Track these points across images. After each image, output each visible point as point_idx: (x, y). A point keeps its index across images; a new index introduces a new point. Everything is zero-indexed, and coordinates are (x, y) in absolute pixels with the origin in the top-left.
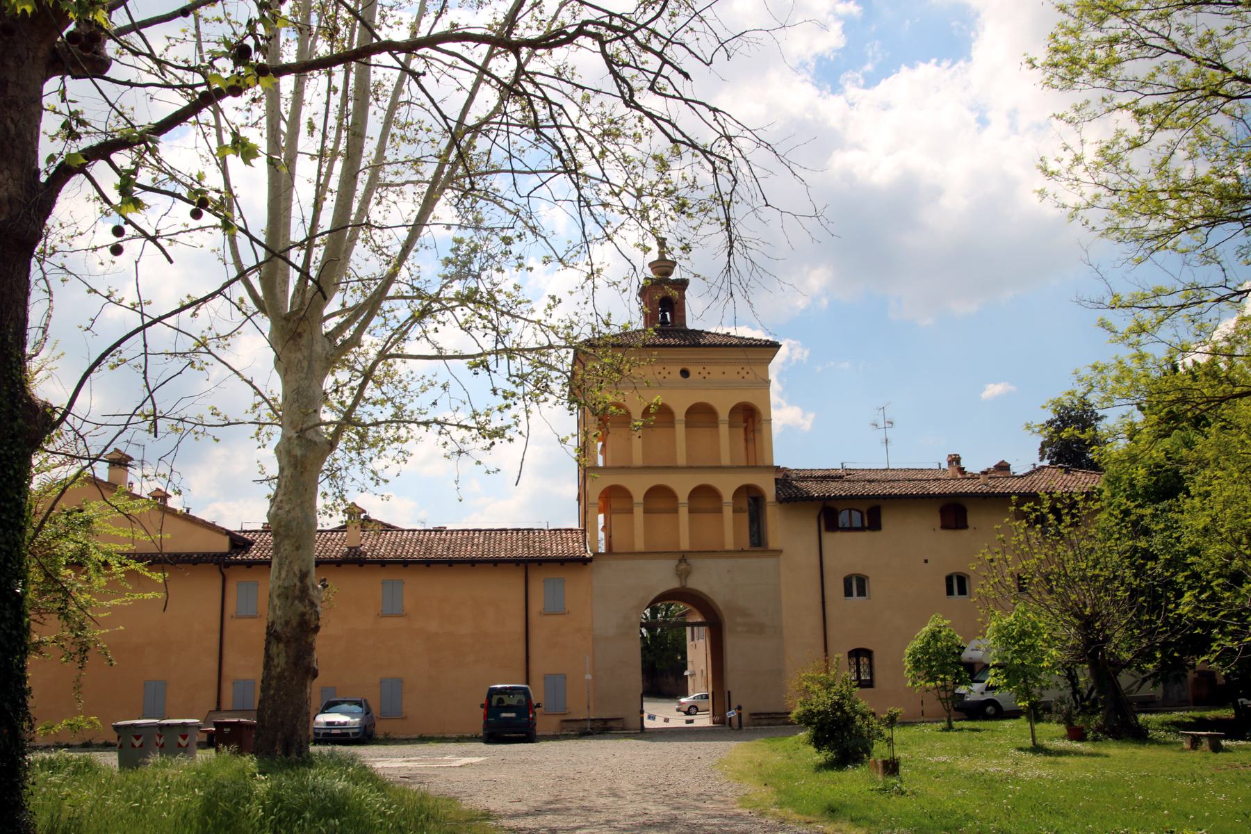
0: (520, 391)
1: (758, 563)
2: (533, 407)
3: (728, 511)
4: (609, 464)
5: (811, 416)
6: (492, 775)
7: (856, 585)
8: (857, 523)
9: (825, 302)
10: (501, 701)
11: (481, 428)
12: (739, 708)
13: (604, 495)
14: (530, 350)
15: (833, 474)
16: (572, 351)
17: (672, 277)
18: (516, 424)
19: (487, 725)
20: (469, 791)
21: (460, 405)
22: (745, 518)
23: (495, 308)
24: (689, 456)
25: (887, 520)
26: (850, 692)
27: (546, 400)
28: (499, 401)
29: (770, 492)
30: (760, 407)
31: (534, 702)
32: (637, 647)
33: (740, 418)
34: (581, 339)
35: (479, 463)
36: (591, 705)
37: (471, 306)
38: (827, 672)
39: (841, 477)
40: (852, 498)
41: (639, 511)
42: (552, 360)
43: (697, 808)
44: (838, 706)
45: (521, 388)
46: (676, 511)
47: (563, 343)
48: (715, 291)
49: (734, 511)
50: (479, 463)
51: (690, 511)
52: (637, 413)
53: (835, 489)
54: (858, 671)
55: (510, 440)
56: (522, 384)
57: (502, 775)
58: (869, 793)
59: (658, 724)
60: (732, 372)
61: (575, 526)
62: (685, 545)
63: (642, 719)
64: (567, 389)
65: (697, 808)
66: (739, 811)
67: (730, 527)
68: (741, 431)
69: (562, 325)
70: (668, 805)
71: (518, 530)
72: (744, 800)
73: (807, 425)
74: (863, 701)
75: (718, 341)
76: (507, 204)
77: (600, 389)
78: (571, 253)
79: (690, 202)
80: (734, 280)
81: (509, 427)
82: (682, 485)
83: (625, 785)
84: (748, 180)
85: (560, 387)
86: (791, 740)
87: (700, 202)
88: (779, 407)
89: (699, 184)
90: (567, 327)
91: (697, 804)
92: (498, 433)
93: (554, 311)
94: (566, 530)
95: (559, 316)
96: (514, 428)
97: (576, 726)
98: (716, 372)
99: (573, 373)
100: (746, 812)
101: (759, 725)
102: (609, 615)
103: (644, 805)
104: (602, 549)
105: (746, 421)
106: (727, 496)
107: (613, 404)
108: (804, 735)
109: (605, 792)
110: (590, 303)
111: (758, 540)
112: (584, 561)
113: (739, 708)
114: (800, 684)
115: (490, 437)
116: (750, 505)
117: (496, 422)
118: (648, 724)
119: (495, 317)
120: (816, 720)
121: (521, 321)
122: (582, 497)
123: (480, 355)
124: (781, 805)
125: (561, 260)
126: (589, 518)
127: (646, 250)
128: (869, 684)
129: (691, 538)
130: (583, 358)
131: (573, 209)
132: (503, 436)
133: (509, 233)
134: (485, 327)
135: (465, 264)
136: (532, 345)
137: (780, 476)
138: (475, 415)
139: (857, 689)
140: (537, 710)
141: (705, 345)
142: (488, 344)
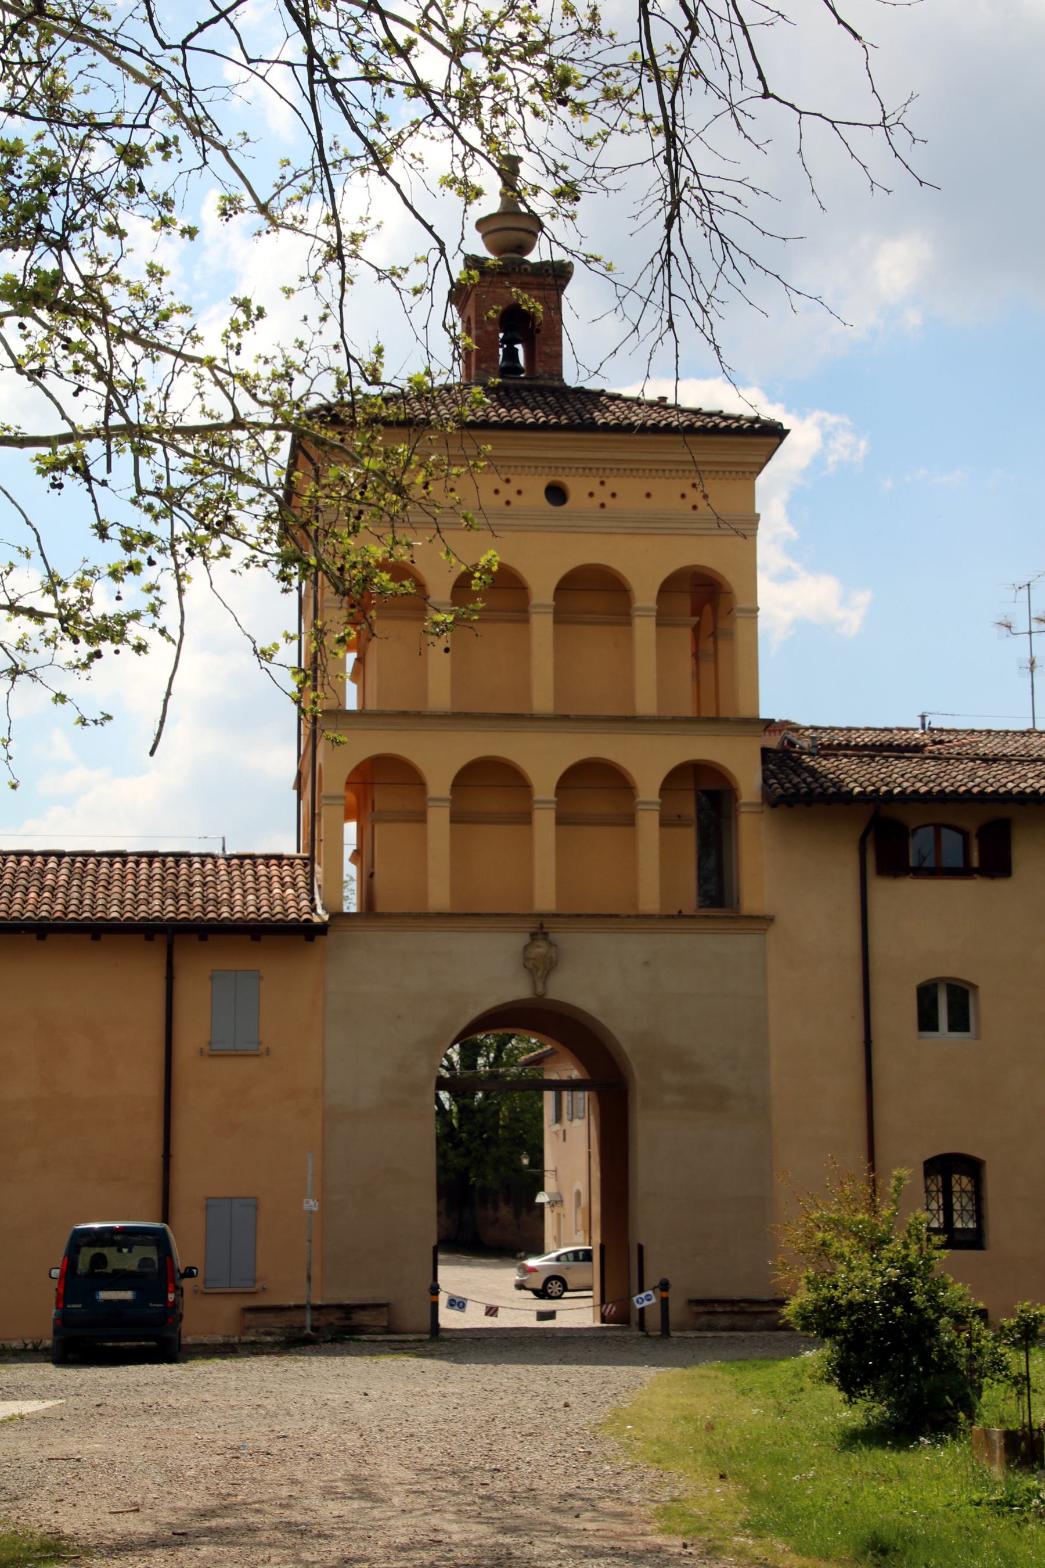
0: (161, 530)
1: (716, 945)
2: (195, 566)
3: (648, 823)
4: (372, 706)
5: (863, 598)
6: (71, 1445)
7: (945, 1004)
8: (952, 857)
9: (913, 318)
10: (99, 1260)
11: (68, 618)
12: (664, 1286)
13: (358, 776)
14: (189, 432)
15: (899, 739)
16: (288, 436)
17: (533, 257)
18: (154, 610)
19: (64, 1322)
20: (12, 1486)
21: (18, 559)
22: (688, 839)
23: (102, 323)
24: (560, 690)
25: (1027, 853)
26: (928, 1260)
27: (225, 553)
28: (113, 553)
29: (749, 780)
30: (732, 579)
31: (180, 1265)
32: (430, 1129)
33: (684, 603)
34: (313, 402)
35: (60, 698)
36: (316, 1271)
37: (43, 314)
38: (874, 1210)
39: (918, 748)
40: (943, 798)
41: (439, 818)
42: (243, 460)
43: (558, 1530)
44: (897, 1292)
45: (164, 523)
46: (629, 821)
47: (266, 416)
48: (632, 305)
49: (664, 823)
50: (60, 698)
51: (561, 821)
52: (440, 590)
53: (902, 776)
54: (948, 1209)
55: (140, 648)
56: (168, 513)
57: (93, 1446)
58: (971, 1510)
59: (472, 1318)
60: (668, 494)
61: (287, 845)
62: (545, 900)
63: (435, 1306)
64: (275, 527)
65: (558, 1530)
66: (660, 1540)
67: (653, 859)
68: (686, 635)
69: (266, 372)
70: (489, 1522)
71: (151, 856)
72: (670, 1513)
73: (853, 621)
74: (958, 1282)
75: (637, 417)
76: (127, 57)
77: (354, 531)
78: (289, 192)
79: (579, 71)
80: (679, 286)
81: (136, 616)
82: (544, 760)
83: (390, 1471)
84: (723, 31)
85: (260, 523)
86: (786, 1366)
87: (607, 72)
88: (785, 577)
89: (604, 27)
90: (276, 377)
91: (561, 1520)
92: (109, 630)
93: (247, 338)
94: (267, 858)
95: (260, 348)
96: (148, 619)
97: (277, 1321)
98: (629, 493)
99: (291, 489)
100: (674, 1543)
101: (710, 1328)
102: (360, 1060)
103: (435, 1520)
104: (351, 904)
105: (697, 611)
106: (648, 789)
107: (383, 566)
108: (816, 1357)
109: (342, 1487)
110: (333, 322)
111: (716, 890)
112: (308, 932)
113: (664, 1286)
114: (809, 1235)
115: (91, 639)
116: (700, 810)
117: (104, 603)
118: (449, 1319)
119: (103, 349)
120: (844, 1324)
121: (168, 359)
122: (307, 780)
123: (65, 439)
124: (758, 1528)
125: (263, 209)
126: (321, 832)
127: (471, 193)
128: (975, 1240)
129: (560, 881)
130: (314, 451)
131: (289, 84)
132: (119, 637)
133: (140, 138)
134: (78, 371)
135: (27, 212)
136: (194, 419)
137: (773, 741)
138: (53, 584)
139: (945, 1254)
140: (186, 1283)
141: (606, 428)
142: (87, 411)
